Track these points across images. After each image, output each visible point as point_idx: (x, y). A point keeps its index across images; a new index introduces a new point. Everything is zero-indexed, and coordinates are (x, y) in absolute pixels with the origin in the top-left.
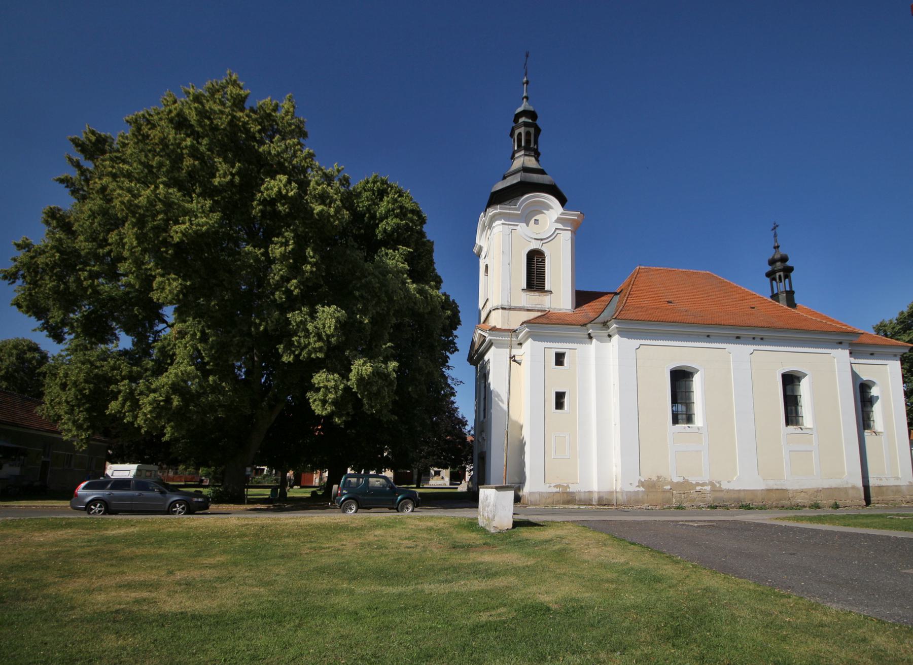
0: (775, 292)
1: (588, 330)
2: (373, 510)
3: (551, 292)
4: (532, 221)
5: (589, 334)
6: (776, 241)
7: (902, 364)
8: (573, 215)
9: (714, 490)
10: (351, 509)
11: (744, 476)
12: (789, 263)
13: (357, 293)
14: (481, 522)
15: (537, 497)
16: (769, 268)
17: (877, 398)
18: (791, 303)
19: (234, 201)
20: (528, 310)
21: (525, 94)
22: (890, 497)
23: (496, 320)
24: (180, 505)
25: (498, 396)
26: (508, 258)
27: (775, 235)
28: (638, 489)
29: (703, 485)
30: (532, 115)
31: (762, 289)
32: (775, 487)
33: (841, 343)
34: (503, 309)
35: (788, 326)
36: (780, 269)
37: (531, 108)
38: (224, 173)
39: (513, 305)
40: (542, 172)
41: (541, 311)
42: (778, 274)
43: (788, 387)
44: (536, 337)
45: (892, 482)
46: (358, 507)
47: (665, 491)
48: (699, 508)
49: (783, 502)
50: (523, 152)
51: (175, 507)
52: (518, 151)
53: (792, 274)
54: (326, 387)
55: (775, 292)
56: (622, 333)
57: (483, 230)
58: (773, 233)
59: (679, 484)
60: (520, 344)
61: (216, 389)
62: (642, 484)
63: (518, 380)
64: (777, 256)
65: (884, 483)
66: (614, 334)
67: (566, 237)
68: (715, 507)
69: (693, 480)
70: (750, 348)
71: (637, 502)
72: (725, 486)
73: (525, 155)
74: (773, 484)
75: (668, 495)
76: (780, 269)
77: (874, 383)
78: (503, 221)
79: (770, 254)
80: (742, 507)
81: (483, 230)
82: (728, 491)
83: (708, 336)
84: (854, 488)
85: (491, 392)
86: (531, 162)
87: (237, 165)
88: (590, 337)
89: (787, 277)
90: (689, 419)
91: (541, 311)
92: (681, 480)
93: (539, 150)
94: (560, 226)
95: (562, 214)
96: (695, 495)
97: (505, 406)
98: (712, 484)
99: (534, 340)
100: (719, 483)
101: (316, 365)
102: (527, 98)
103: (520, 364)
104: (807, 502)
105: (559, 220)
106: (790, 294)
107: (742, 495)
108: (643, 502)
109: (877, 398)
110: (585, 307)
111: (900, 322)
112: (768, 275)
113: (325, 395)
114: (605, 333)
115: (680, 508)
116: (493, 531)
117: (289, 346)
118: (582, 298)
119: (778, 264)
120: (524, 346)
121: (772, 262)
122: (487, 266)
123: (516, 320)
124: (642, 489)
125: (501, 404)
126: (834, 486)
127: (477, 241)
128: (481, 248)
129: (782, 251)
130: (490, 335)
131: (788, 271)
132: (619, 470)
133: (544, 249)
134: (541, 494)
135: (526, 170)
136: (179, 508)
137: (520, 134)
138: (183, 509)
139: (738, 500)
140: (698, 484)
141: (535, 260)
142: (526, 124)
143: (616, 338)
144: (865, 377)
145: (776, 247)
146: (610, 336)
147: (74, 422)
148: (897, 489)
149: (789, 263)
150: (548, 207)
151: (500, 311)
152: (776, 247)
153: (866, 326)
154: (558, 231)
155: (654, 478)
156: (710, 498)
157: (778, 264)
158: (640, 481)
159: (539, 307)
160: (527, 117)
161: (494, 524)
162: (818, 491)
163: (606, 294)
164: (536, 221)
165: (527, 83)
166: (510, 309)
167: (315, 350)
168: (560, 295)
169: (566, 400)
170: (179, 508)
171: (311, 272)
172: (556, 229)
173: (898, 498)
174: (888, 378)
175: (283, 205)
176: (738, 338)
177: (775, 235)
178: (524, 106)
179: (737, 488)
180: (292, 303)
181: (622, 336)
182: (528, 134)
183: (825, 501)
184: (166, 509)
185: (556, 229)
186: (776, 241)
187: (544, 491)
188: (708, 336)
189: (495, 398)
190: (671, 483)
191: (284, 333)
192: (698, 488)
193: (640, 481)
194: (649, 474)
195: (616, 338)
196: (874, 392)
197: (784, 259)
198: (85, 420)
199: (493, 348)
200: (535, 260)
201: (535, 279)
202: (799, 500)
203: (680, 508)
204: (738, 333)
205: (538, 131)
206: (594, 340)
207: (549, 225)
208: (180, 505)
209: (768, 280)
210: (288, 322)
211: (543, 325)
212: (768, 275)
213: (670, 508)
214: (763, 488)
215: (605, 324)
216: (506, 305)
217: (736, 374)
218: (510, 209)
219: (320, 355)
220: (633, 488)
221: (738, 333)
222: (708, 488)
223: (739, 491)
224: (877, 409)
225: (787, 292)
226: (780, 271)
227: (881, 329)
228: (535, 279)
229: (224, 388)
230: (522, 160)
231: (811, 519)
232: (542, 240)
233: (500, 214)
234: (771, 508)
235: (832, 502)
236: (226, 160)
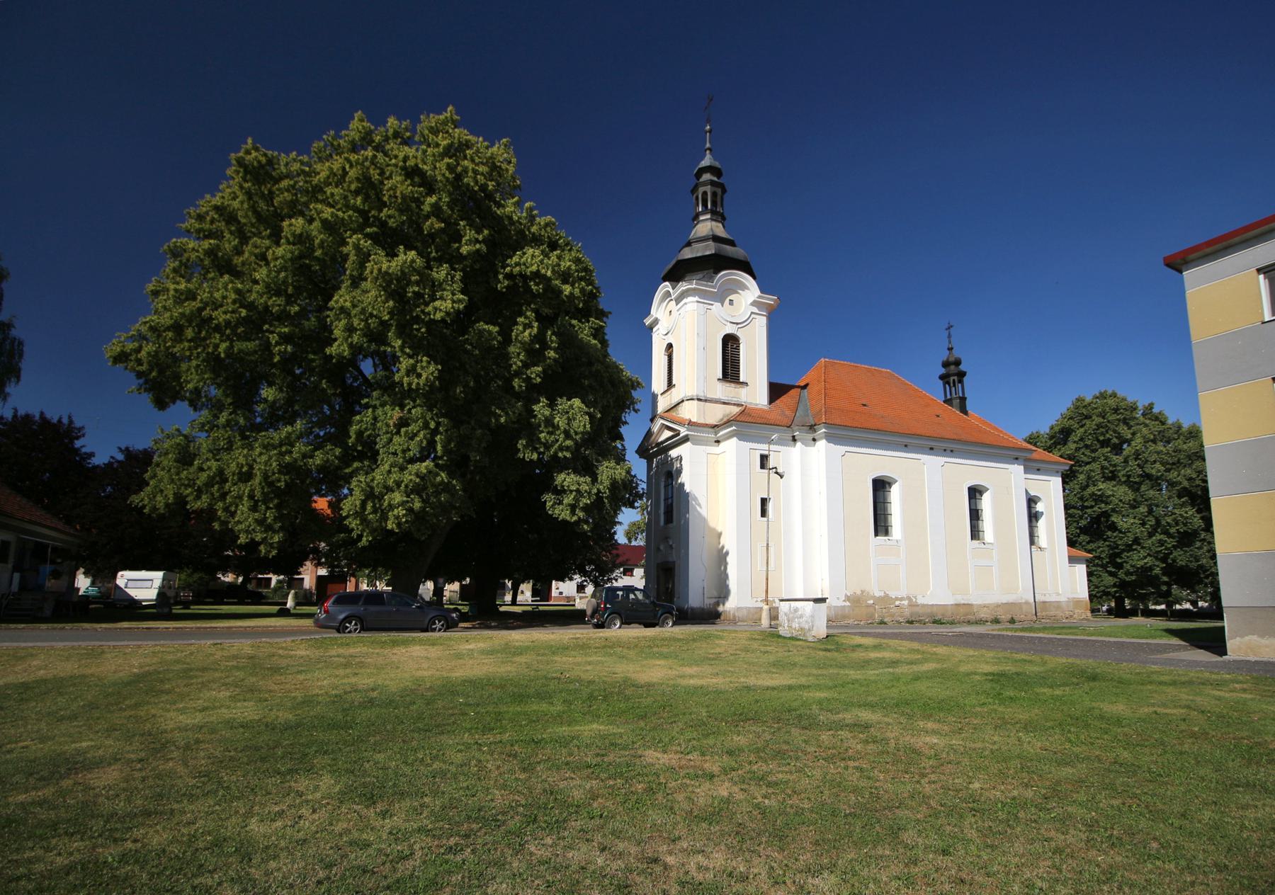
4: (727, 301)
8: (770, 300)
9: (912, 605)
11: (936, 589)
12: (962, 367)
15: (745, 612)
16: (943, 371)
18: (964, 410)
19: (478, 274)
21: (708, 145)
23: (689, 412)
25: (695, 499)
26: (693, 339)
27: (949, 336)
29: (902, 599)
34: (699, 400)
35: (973, 439)
36: (953, 374)
37: (717, 164)
38: (470, 242)
39: (710, 396)
41: (738, 405)
44: (742, 436)
45: (1053, 599)
46: (622, 623)
49: (970, 617)
50: (708, 216)
52: (703, 213)
53: (965, 379)
54: (578, 491)
56: (830, 438)
57: (663, 300)
60: (718, 442)
63: (715, 479)
64: (952, 359)
67: (761, 324)
68: (911, 622)
69: (893, 594)
71: (845, 617)
72: (921, 601)
73: (712, 219)
74: (960, 599)
75: (871, 609)
76: (953, 374)
77: (1039, 499)
78: (697, 298)
79: (944, 355)
80: (935, 622)
81: (663, 300)
82: (924, 606)
84: (1027, 603)
85: (686, 497)
86: (719, 230)
87: (486, 232)
88: (794, 439)
89: (961, 381)
90: (886, 533)
91: (738, 405)
98: (909, 598)
101: (559, 465)
104: (989, 617)
105: (754, 303)
107: (935, 609)
111: (1052, 438)
112: (941, 377)
113: (576, 500)
114: (811, 436)
115: (882, 623)
116: (810, 639)
117: (533, 443)
118: (776, 391)
119: (952, 367)
123: (715, 414)
124: (848, 604)
127: (653, 311)
128: (656, 321)
129: (957, 354)
131: (962, 375)
133: (739, 334)
135: (716, 239)
136: (438, 625)
137: (705, 193)
139: (931, 615)
140: (897, 599)
141: (730, 343)
142: (712, 183)
143: (822, 444)
144: (1032, 493)
145: (950, 349)
146: (814, 440)
147: (260, 522)
148: (1057, 605)
149: (962, 367)
150: (744, 287)
152: (950, 349)
153: (1018, 436)
155: (859, 592)
156: (907, 613)
157: (952, 367)
159: (735, 400)
160: (712, 174)
161: (813, 633)
162: (998, 606)
163: (792, 387)
164: (731, 302)
165: (710, 131)
167: (561, 449)
169: (770, 507)
170: (438, 625)
171: (555, 360)
173: (1059, 614)
174: (1051, 492)
175: (537, 284)
177: (949, 336)
180: (533, 393)
181: (829, 441)
182: (714, 194)
189: (692, 502)
190: (874, 597)
191: (526, 426)
194: (855, 589)
195: (822, 444)
196: (1039, 507)
197: (958, 363)
198: (275, 519)
200: (730, 343)
201: (730, 371)
202: (983, 615)
203: (882, 623)
204: (932, 444)
206: (799, 444)
207: (744, 306)
211: (745, 423)
212: (941, 377)
214: (952, 602)
215: (812, 428)
216: (701, 395)
217: (929, 483)
219: (568, 455)
221: (932, 444)
222: (906, 603)
224: (1042, 523)
227: (1033, 440)
228: (730, 371)
231: (1011, 630)
233: (694, 289)
236: (471, 225)
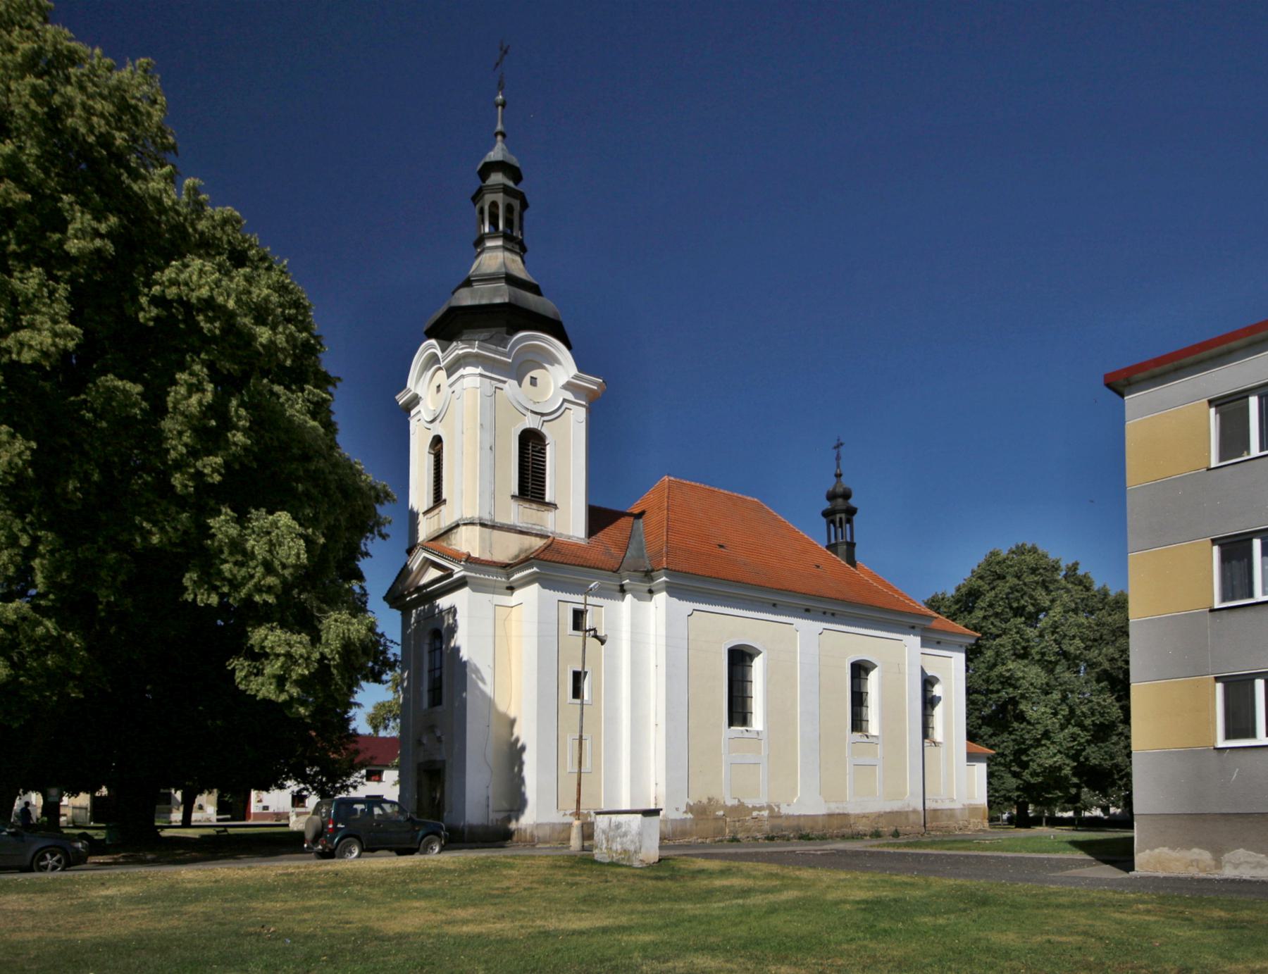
0: (833, 541)
1: (622, 579)
2: (379, 853)
3: (554, 506)
4: (527, 379)
5: (622, 586)
6: (838, 466)
7: (968, 660)
8: (592, 383)
9: (774, 815)
10: (351, 853)
11: (805, 800)
13: (300, 487)
14: (599, 855)
15: (547, 830)
16: (827, 505)
17: (939, 698)
18: (851, 561)
20: (521, 532)
21: (499, 127)
22: (944, 823)
24: (53, 855)
25: (477, 671)
26: (469, 432)
27: (838, 458)
28: (685, 816)
29: (760, 809)
30: (513, 172)
31: (816, 534)
32: (837, 811)
33: (913, 627)
34: (483, 525)
36: (840, 511)
37: (514, 161)
38: (84, 232)
39: (500, 520)
40: (535, 289)
42: (838, 516)
43: (856, 681)
45: (947, 805)
46: (362, 850)
47: (717, 819)
48: (755, 839)
51: (45, 859)
55: (833, 541)
56: (673, 591)
58: (835, 452)
59: (733, 809)
61: (56, 644)
62: (690, 809)
64: (840, 490)
65: (939, 806)
66: (660, 591)
67: (577, 417)
69: (749, 803)
70: (819, 626)
71: (684, 834)
72: (785, 810)
74: (835, 808)
75: (721, 823)
76: (840, 511)
78: (479, 370)
79: (830, 484)
82: (788, 817)
83: (774, 605)
86: (517, 267)
88: (623, 590)
89: (849, 521)
92: (736, 802)
93: (526, 243)
94: (570, 396)
95: (576, 377)
96: (750, 823)
97: (488, 689)
98: (770, 808)
99: (544, 587)
100: (778, 806)
102: (504, 135)
103: (603, 642)
104: (868, 829)
105: (568, 386)
106: (851, 545)
108: (691, 834)
109: (939, 698)
110: (600, 535)
112: (826, 514)
113: (286, 669)
114: (646, 587)
117: (209, 577)
118: (598, 519)
120: (517, 593)
121: (831, 497)
122: (437, 441)
124: (690, 816)
125: (481, 685)
126: (896, 809)
127: (411, 383)
129: (846, 482)
130: (466, 569)
132: (662, 789)
134: (553, 825)
136: (50, 861)
138: (59, 861)
139: (798, 829)
140: (754, 808)
142: (506, 190)
143: (661, 598)
144: (929, 673)
145: (838, 476)
146: (651, 592)
150: (554, 360)
151: (478, 528)
152: (838, 476)
154: (566, 405)
155: (705, 801)
156: (766, 826)
157: (840, 501)
158: (688, 805)
160: (505, 173)
161: (641, 856)
164: (534, 381)
165: (504, 105)
166: (493, 527)
167: (259, 589)
168: (568, 518)
170: (50, 861)
172: (565, 400)
173: (952, 824)
174: (952, 670)
176: (807, 610)
177: (838, 458)
178: (497, 153)
179: (797, 813)
180: (206, 498)
182: (509, 209)
183: (886, 829)
184: (28, 863)
185: (565, 400)
186: (838, 466)
187: (556, 821)
188: (774, 605)
189: (472, 676)
190: (724, 807)
191: (197, 552)
192: (755, 814)
193: (688, 805)
194: (700, 795)
195: (661, 598)
196: (937, 690)
197: (847, 495)
199: (466, 590)
201: (531, 485)
202: (862, 827)
203: (734, 840)
205: (524, 205)
206: (629, 597)
208: (53, 855)
209: (824, 520)
210: (206, 531)
211: (550, 564)
212: (826, 514)
213: (721, 841)
215: (648, 575)
216: (487, 517)
218: (496, 352)
219: (271, 599)
220: (679, 815)
222: (765, 813)
223: (799, 816)
224: (938, 711)
225: (847, 543)
226: (841, 511)
227: (934, 604)
229: (71, 643)
230: (495, 258)
231: (894, 845)
232: (542, 415)
233: (477, 356)
234: (831, 837)
235: (893, 829)
236: (85, 204)
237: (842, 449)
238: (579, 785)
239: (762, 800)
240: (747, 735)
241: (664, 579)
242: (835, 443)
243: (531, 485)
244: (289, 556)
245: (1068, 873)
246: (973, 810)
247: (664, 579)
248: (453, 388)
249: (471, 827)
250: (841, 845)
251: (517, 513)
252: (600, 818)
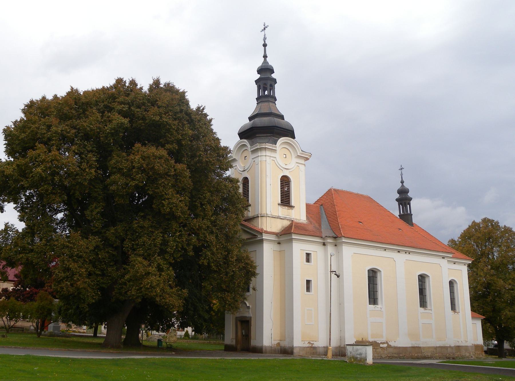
29: (383, 343)
32: (416, 345)
82: (396, 348)
140: (381, 343)
237: (403, 170)
238: (330, 332)
239: (384, 340)
240: (376, 309)
241: (103, 327)
242: (400, 168)
243: (286, 199)
244: (147, 284)
245: (71, 339)
246: (477, 347)
247: (103, 327)
248: (254, 160)
249: (266, 347)
250: (75, 339)
251: (283, 211)
252: (348, 347)
